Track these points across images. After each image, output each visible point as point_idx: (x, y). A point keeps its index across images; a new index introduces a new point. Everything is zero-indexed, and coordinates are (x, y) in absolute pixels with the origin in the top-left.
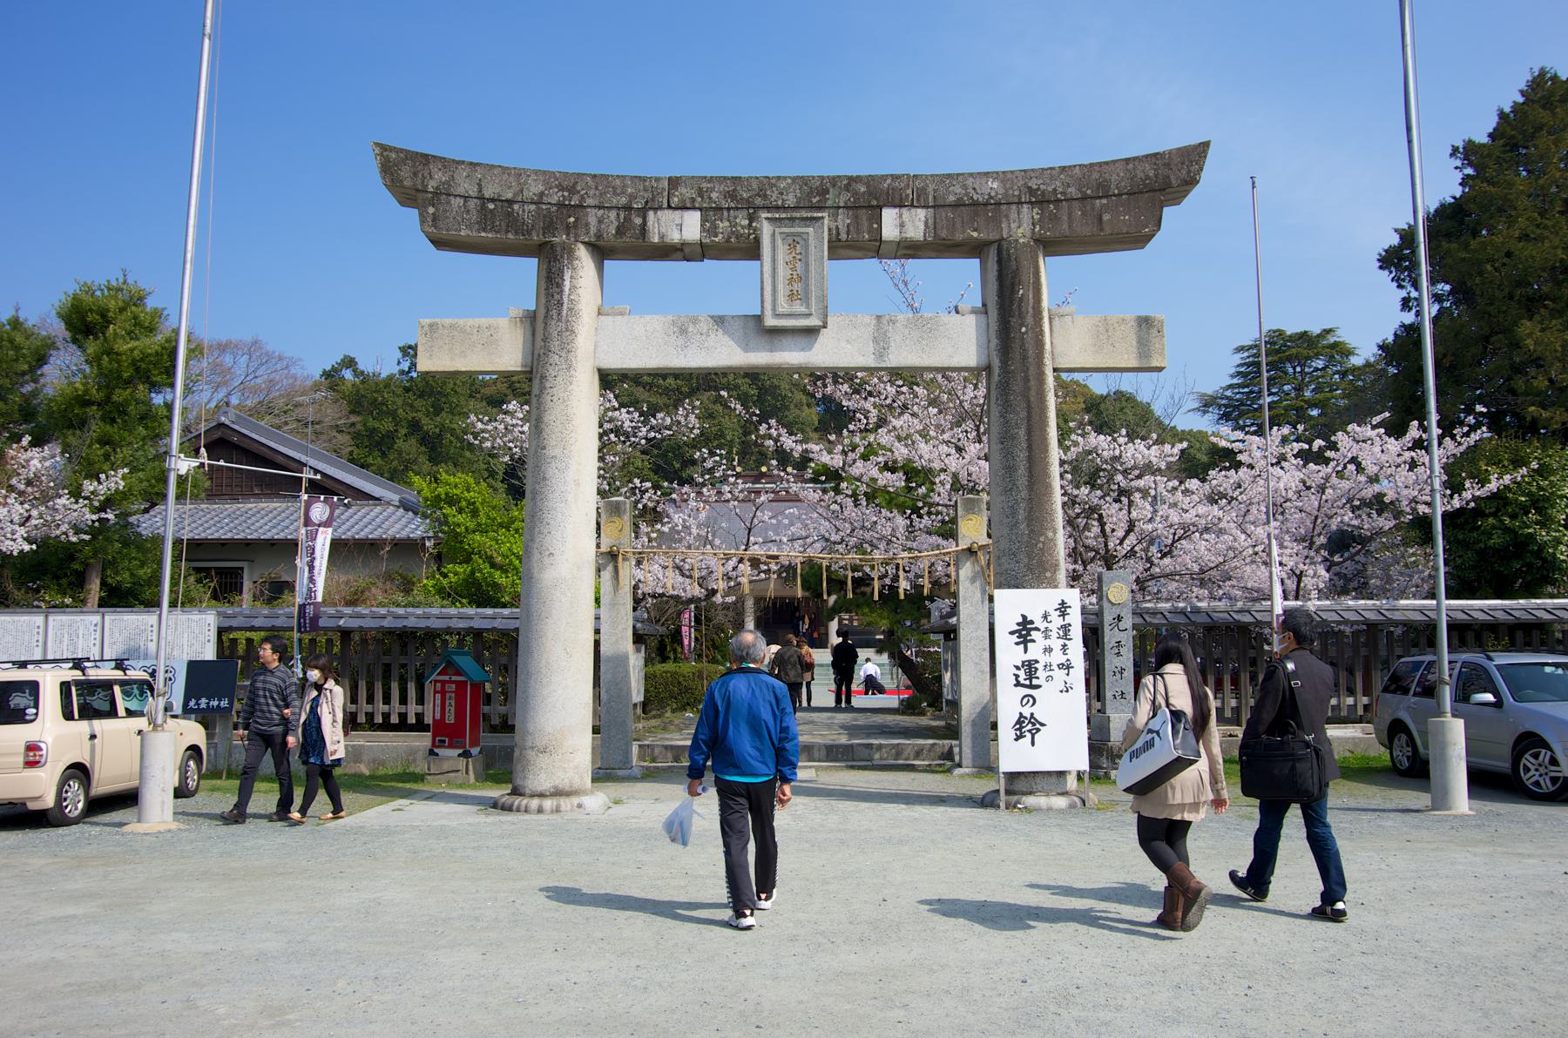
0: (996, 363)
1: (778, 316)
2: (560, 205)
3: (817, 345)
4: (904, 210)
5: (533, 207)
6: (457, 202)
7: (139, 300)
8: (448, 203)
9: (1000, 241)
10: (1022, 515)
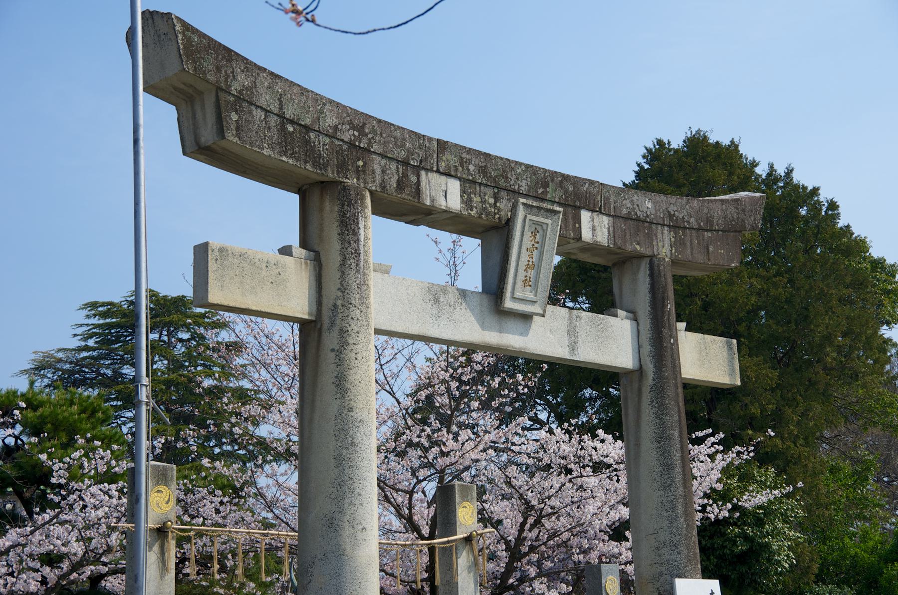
0: (650, 368)
1: (513, 298)
2: (351, 144)
3: (531, 332)
4: (595, 214)
5: (327, 140)
6: (259, 114)
7: (649, 150)
8: (250, 112)
9: (652, 257)
10: (680, 510)
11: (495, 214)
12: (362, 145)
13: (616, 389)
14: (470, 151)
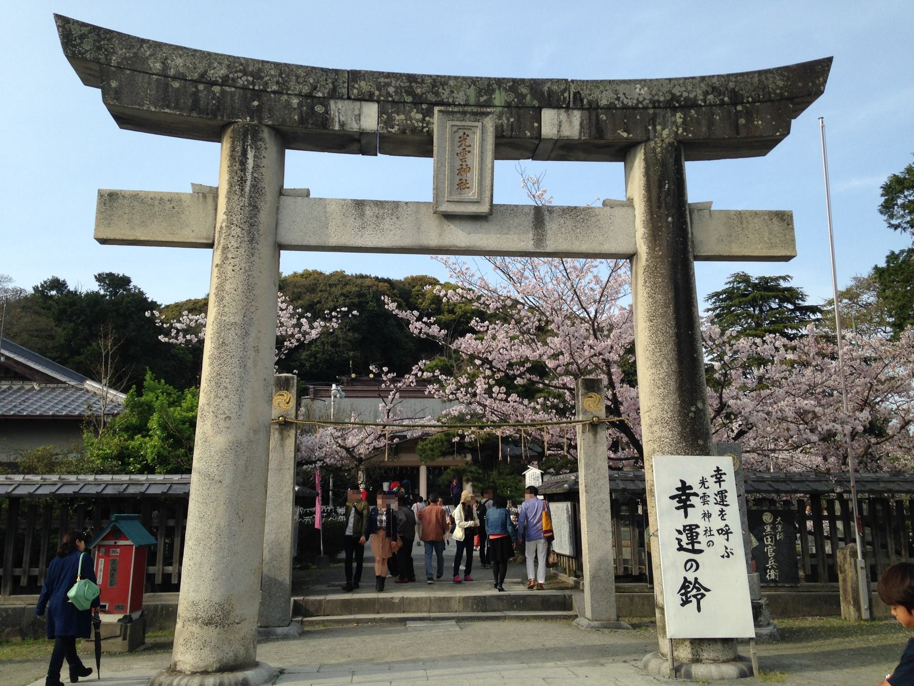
11: (423, 127)
12: (257, 88)
13: (792, 328)
14: (389, 75)
